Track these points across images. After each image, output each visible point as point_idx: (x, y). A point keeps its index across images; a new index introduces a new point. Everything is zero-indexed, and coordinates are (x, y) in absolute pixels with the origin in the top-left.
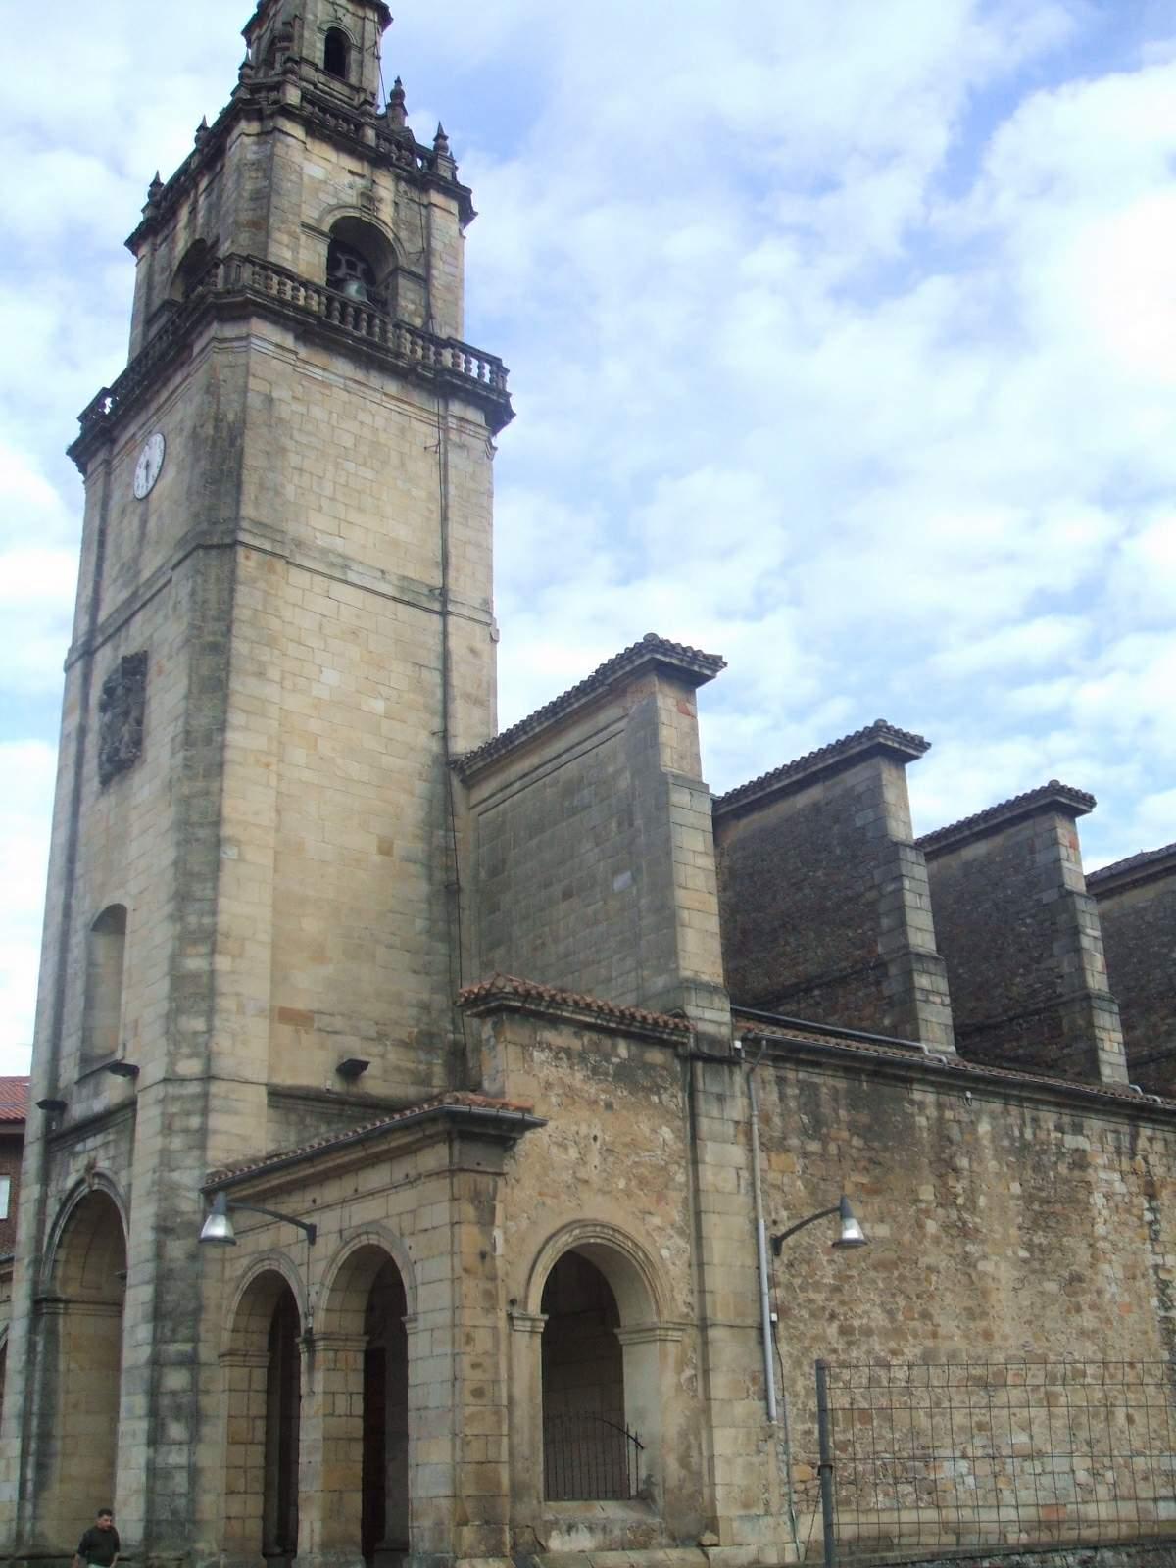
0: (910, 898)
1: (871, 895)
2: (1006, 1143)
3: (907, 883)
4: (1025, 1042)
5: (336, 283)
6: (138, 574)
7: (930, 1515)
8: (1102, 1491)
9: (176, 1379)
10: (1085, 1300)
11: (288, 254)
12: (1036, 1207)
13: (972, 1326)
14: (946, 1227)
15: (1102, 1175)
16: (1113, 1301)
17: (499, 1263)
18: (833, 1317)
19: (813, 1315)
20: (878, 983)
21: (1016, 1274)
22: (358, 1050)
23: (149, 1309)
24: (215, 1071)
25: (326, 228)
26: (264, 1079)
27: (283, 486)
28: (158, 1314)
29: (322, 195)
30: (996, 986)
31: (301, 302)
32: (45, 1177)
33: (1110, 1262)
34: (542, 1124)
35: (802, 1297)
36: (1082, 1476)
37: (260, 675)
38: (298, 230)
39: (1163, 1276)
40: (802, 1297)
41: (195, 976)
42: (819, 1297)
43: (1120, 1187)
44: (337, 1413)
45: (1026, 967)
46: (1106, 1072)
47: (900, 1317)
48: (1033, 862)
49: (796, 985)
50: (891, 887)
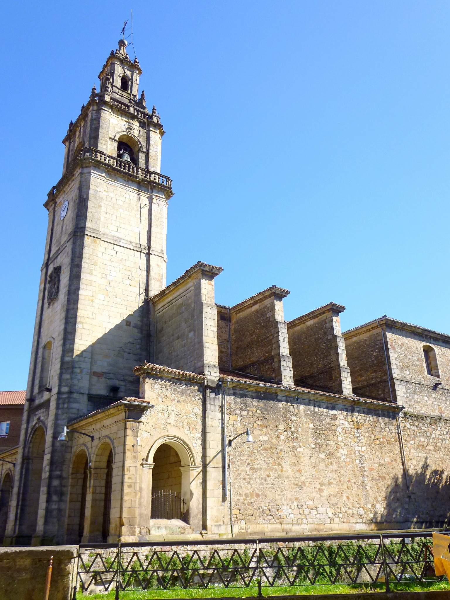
0: (281, 338)
1: (271, 337)
2: (309, 412)
3: (280, 334)
4: (322, 381)
5: (120, 156)
6: (60, 242)
7: (279, 526)
8: (337, 520)
9: (56, 483)
10: (333, 460)
11: (105, 147)
12: (318, 432)
13: (295, 468)
14: (287, 437)
15: (342, 422)
16: (344, 461)
17: (139, 447)
18: (248, 464)
19: (242, 464)
20: (272, 364)
21: (311, 452)
22: (117, 383)
23: (49, 461)
24: (72, 391)
25: (117, 138)
26: (87, 392)
27: (100, 217)
28: (52, 463)
29: (116, 129)
30: (315, 364)
31: (107, 162)
32: (28, 422)
33: (343, 449)
34: (153, 407)
35: (238, 458)
36: (331, 515)
37: (91, 273)
38: (108, 139)
39: (361, 453)
40: (238, 458)
41: (68, 363)
42: (244, 458)
43: (347, 426)
44: (97, 492)
45: (323, 358)
46: (345, 391)
47: (271, 465)
48: (326, 326)
49: (250, 364)
50: (276, 335)
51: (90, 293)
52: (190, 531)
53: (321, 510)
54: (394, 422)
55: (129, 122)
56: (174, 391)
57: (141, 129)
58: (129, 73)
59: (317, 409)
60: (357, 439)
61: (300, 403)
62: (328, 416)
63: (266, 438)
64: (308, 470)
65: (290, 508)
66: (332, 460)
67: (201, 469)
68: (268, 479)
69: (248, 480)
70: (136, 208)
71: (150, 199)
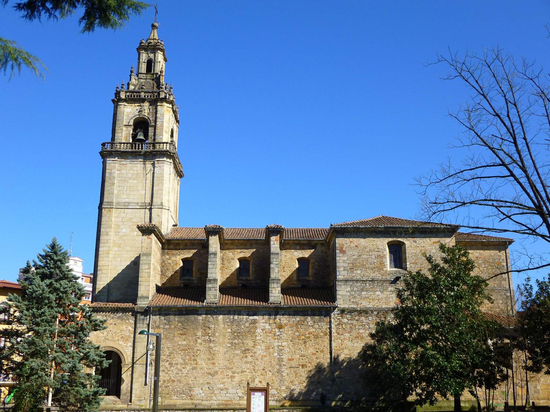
2: (228, 320)
7: (190, 401)
18: (167, 361)
37: (107, 235)
51: (107, 249)
52: (120, 403)
53: (230, 391)
54: (327, 319)
55: (140, 106)
56: (112, 318)
57: (151, 107)
58: (152, 56)
59: (236, 317)
60: (279, 338)
61: (220, 314)
62: (248, 321)
63: (185, 343)
64: (221, 361)
65: (202, 389)
66: (247, 355)
67: (130, 365)
68: (183, 370)
69: (166, 371)
70: (142, 176)
71: (153, 164)
